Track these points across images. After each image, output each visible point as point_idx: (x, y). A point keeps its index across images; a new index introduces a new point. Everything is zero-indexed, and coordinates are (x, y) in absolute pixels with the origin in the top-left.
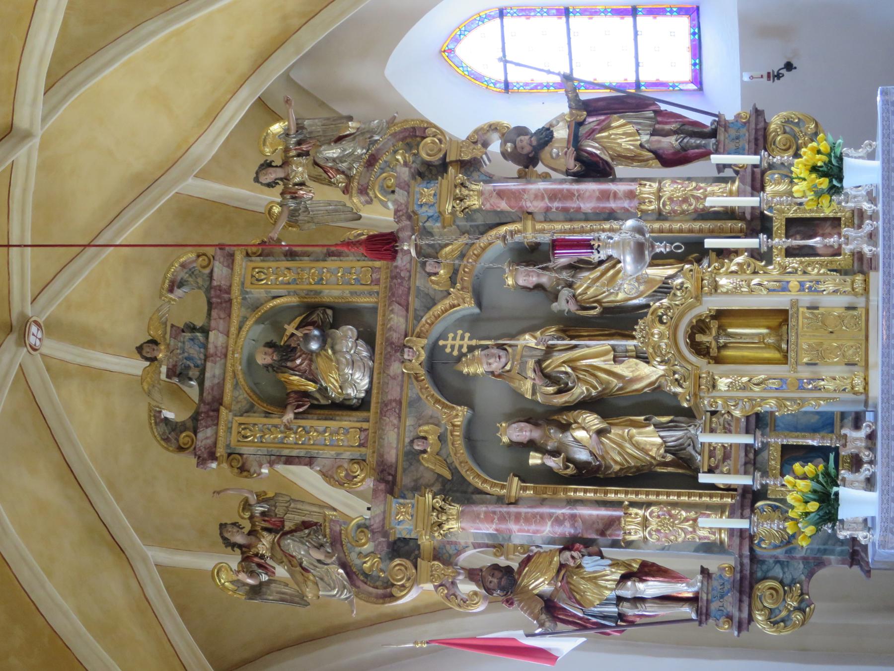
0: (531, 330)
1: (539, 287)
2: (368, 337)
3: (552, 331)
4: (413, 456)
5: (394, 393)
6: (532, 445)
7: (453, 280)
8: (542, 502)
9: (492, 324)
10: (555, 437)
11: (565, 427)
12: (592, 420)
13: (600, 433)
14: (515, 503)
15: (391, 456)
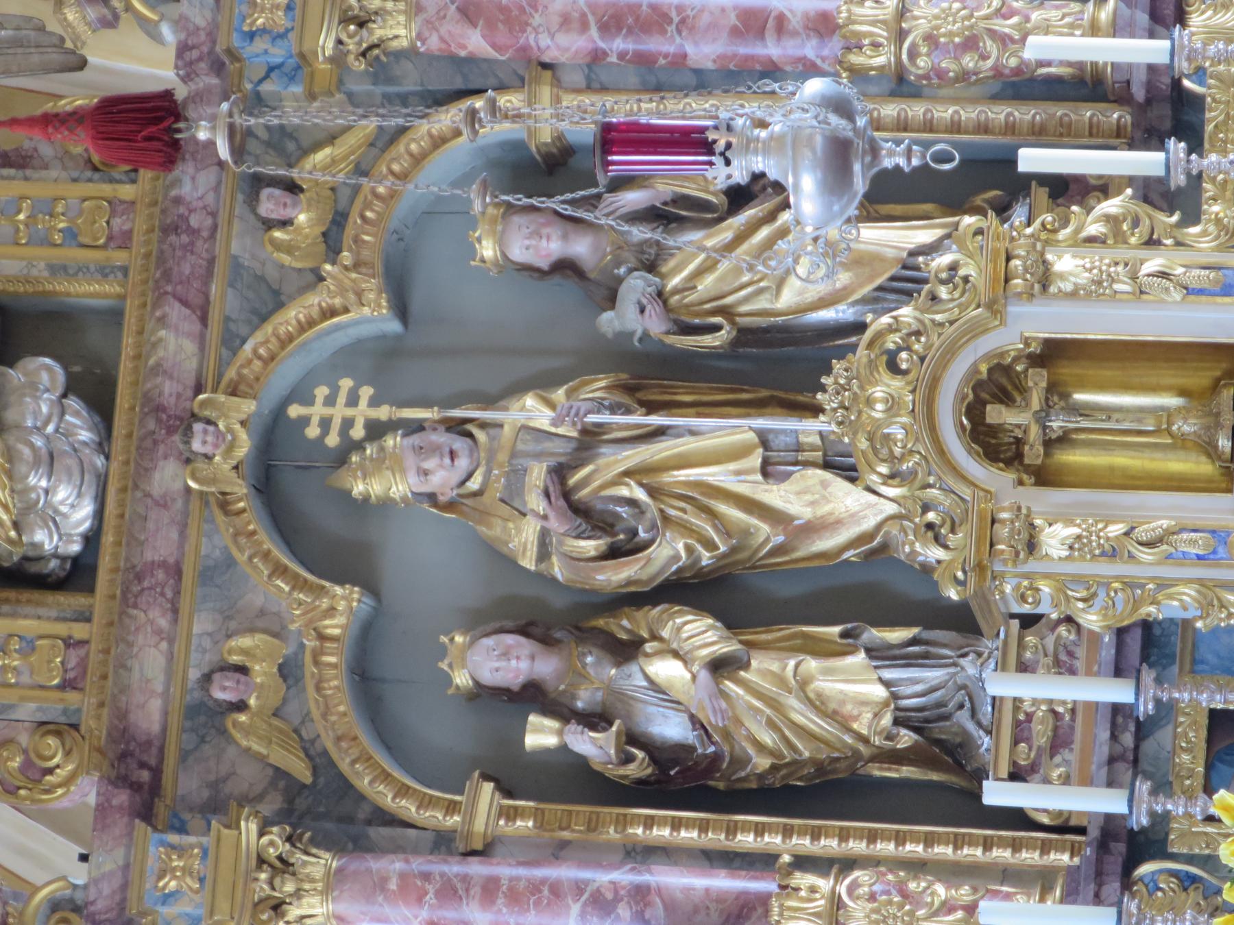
0: (542, 383)
1: (565, 267)
2: (94, 390)
3: (598, 387)
4: (208, 718)
5: (161, 544)
6: (533, 696)
7: (331, 241)
8: (559, 851)
9: (434, 361)
10: (598, 676)
11: (626, 650)
12: (700, 633)
13: (720, 667)
14: (484, 852)
15: (149, 715)
